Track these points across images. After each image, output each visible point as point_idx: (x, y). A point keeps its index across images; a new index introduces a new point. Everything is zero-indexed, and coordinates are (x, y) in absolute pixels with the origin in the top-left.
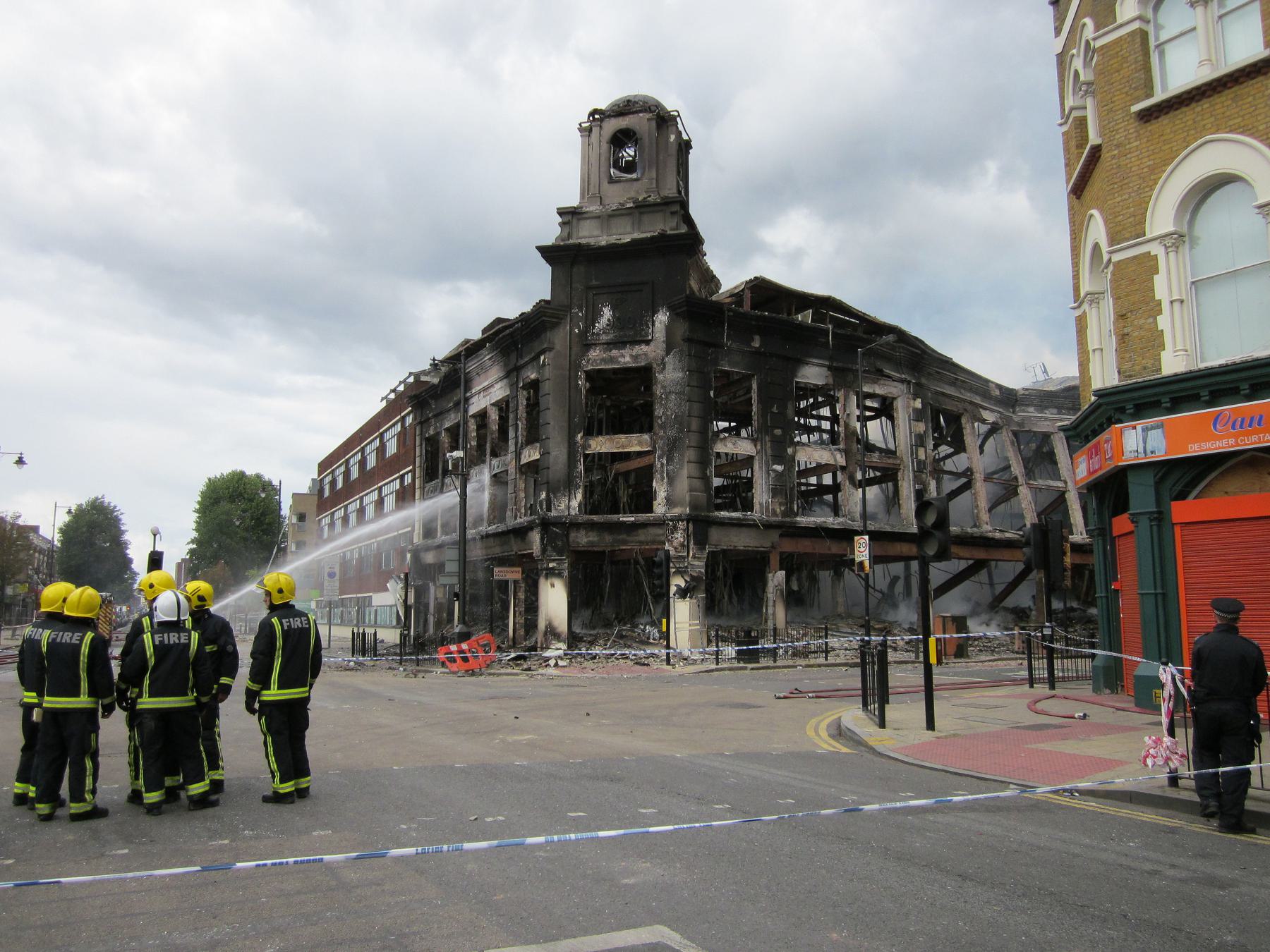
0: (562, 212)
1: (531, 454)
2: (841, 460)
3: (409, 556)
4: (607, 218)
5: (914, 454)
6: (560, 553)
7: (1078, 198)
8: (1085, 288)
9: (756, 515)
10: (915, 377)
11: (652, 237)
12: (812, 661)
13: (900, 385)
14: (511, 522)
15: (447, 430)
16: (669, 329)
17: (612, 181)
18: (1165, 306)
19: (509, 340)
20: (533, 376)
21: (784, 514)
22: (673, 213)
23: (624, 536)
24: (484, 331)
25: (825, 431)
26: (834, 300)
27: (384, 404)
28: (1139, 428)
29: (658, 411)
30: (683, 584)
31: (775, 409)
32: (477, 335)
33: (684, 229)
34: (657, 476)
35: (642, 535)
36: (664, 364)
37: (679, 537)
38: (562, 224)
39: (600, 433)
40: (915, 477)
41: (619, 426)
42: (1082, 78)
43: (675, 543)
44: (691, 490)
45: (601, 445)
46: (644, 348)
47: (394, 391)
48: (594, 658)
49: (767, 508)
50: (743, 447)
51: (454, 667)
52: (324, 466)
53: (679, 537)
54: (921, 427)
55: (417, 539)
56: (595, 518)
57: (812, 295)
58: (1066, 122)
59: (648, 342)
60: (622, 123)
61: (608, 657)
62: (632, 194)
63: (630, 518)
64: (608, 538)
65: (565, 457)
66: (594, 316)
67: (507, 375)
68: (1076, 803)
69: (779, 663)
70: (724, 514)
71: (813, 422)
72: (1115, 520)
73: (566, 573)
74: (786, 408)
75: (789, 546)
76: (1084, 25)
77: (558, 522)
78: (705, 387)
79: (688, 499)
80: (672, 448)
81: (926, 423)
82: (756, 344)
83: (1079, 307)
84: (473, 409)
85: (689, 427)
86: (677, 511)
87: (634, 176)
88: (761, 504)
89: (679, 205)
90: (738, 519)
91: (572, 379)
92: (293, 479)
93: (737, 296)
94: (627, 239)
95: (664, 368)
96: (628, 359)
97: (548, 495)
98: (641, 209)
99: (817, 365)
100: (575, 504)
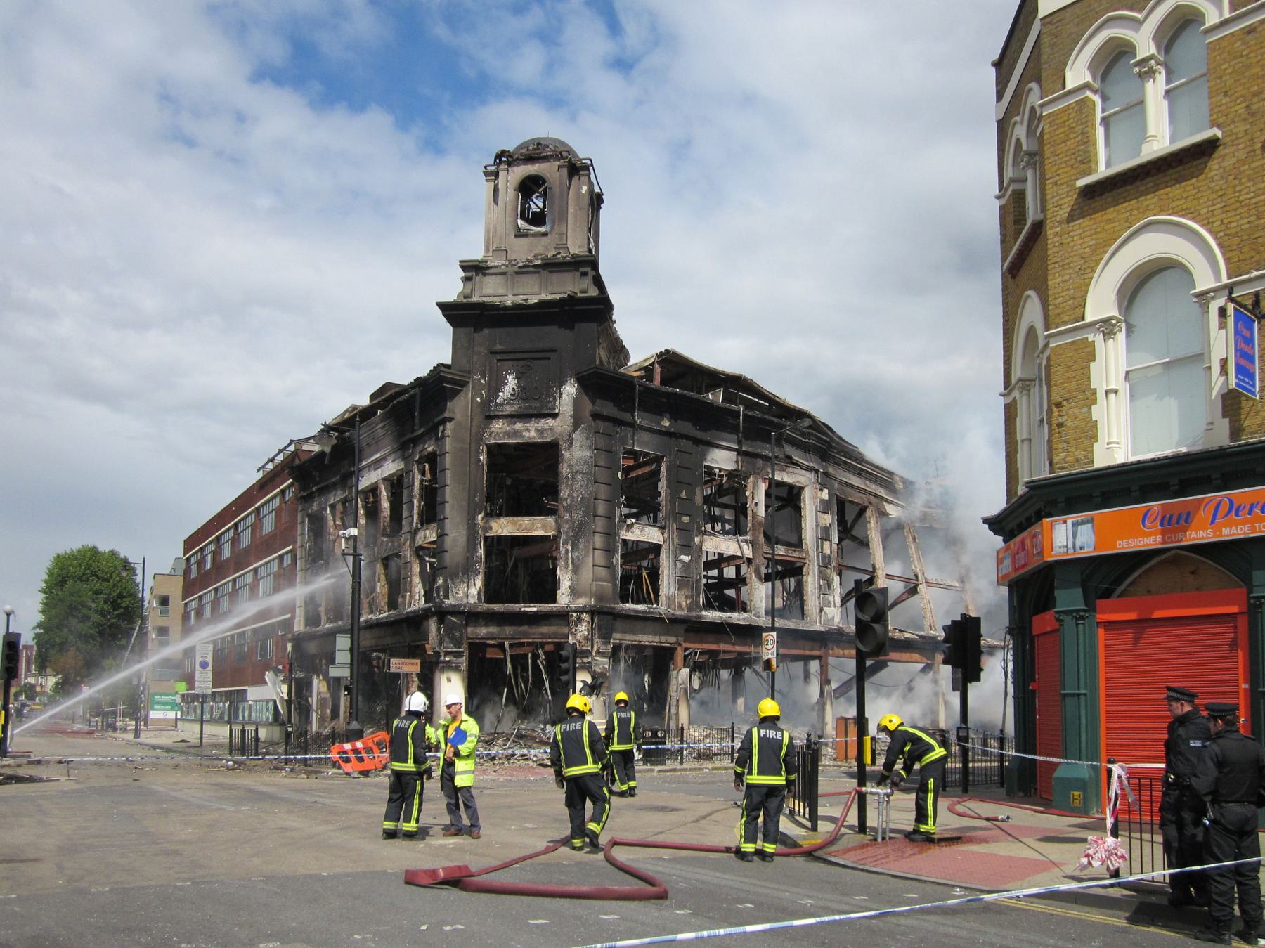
0: (465, 266)
2: (748, 552)
3: (289, 646)
5: (819, 549)
7: (1014, 277)
8: (1017, 373)
9: (662, 608)
10: (823, 467)
11: (562, 300)
12: (718, 764)
13: (808, 474)
16: (576, 402)
17: (520, 234)
18: (1100, 395)
19: (409, 411)
20: (430, 449)
21: (690, 608)
23: (525, 628)
24: (373, 397)
25: (728, 521)
26: (745, 379)
28: (1069, 522)
29: (564, 493)
30: (589, 681)
31: (683, 495)
32: (364, 402)
33: (594, 292)
34: (561, 563)
36: (571, 441)
37: (583, 629)
38: (466, 279)
39: (499, 515)
40: (820, 572)
41: (517, 509)
42: (1024, 147)
43: (579, 636)
45: (504, 527)
46: (550, 422)
47: (272, 460)
48: (493, 759)
50: (651, 535)
51: (348, 768)
52: (190, 543)
53: (583, 629)
54: (827, 519)
55: (299, 627)
56: (497, 607)
57: (723, 373)
58: (1003, 196)
59: (554, 416)
60: (532, 169)
61: (509, 757)
65: (465, 539)
66: (499, 384)
68: (1021, 904)
69: (685, 766)
70: (630, 606)
71: (717, 511)
72: (1036, 619)
73: (464, 667)
74: (695, 494)
76: (1030, 90)
77: (455, 611)
78: (612, 468)
81: (832, 515)
83: (1009, 394)
85: (595, 510)
86: (582, 602)
87: (543, 229)
89: (588, 264)
90: (644, 612)
92: (156, 558)
94: (534, 300)
96: (533, 433)
97: (445, 581)
98: (551, 266)
100: (474, 591)
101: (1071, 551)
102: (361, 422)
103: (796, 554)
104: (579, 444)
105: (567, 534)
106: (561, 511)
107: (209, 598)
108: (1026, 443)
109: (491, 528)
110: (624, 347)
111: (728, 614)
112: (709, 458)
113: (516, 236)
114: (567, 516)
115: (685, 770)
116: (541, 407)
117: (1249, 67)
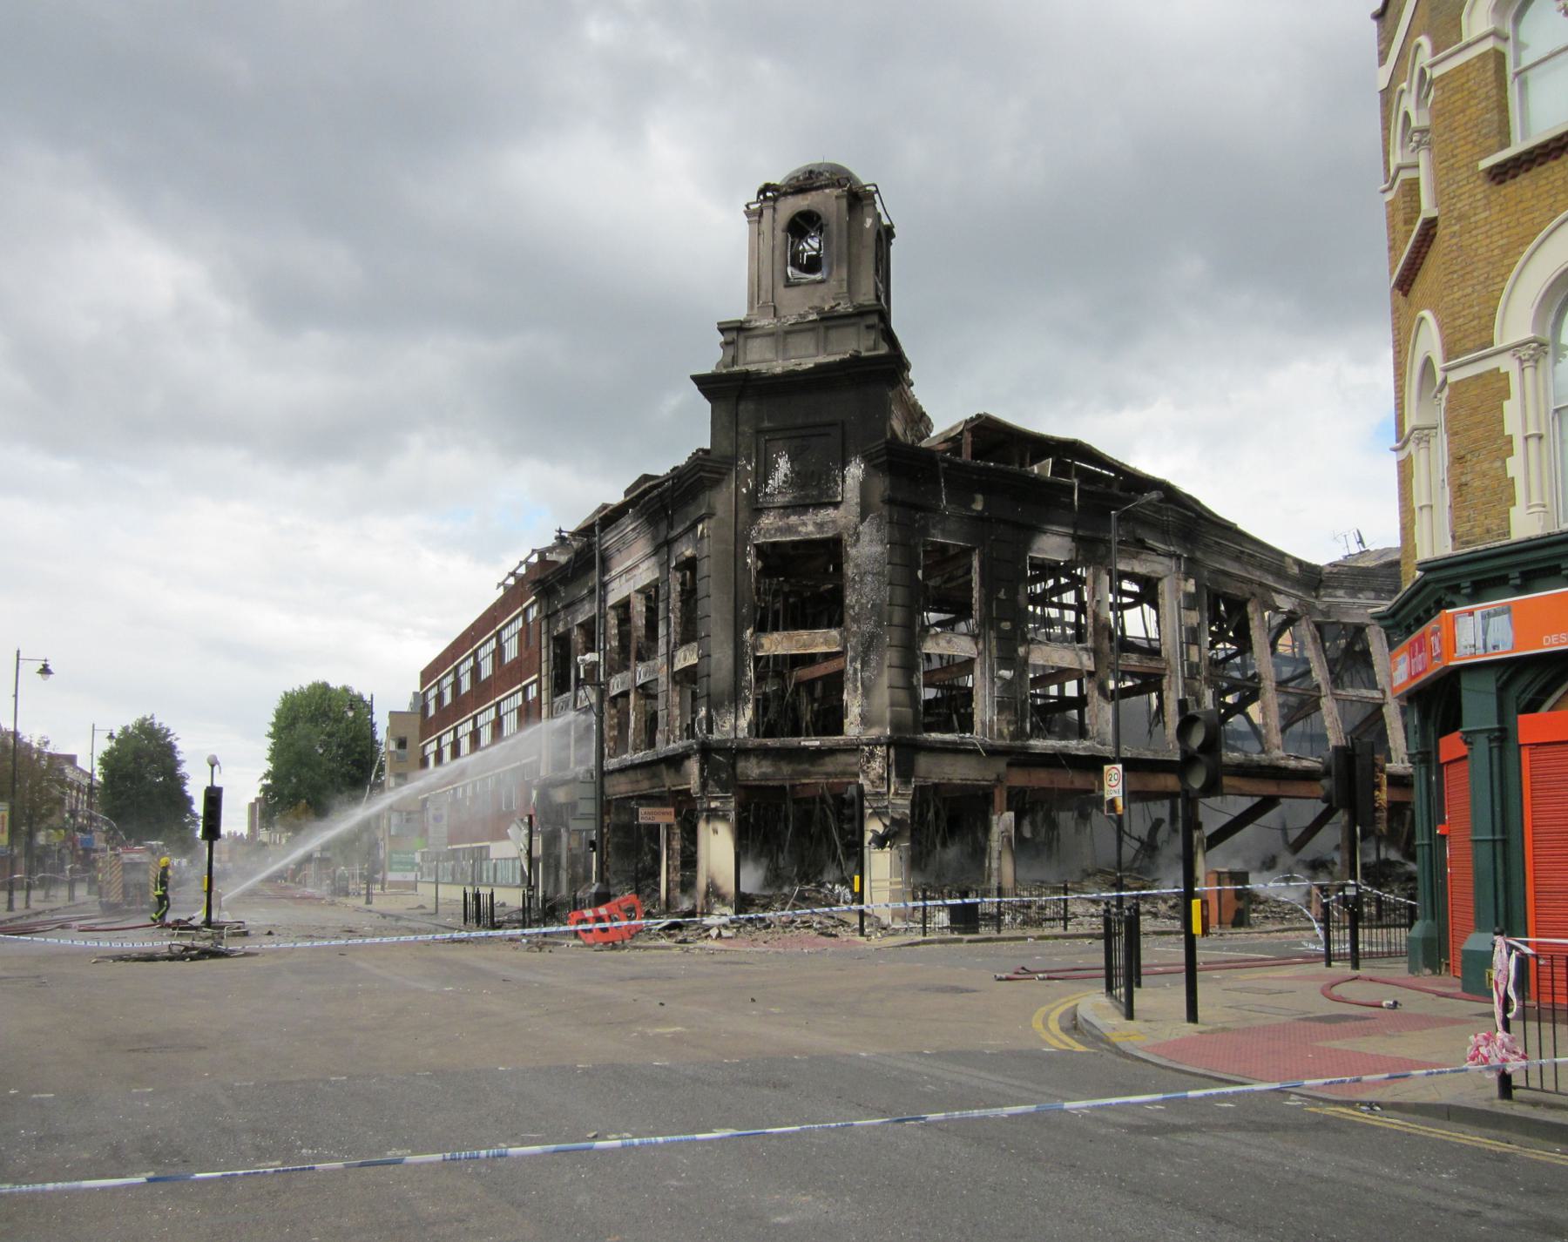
1: (686, 658)
2: (1088, 663)
4: (783, 337)
6: (724, 788)
7: (1405, 294)
9: (976, 737)
10: (1187, 551)
11: (842, 361)
12: (1047, 932)
13: (1166, 561)
15: (581, 625)
16: (864, 487)
17: (789, 284)
20: (688, 553)
21: (1014, 736)
22: (869, 327)
23: (806, 766)
24: (627, 493)
25: (1069, 624)
27: (501, 592)
28: (1478, 614)
29: (850, 598)
30: (881, 830)
31: (1002, 595)
32: (617, 498)
33: (883, 350)
34: (848, 686)
35: (830, 765)
36: (858, 535)
39: (776, 629)
42: (1414, 124)
43: (872, 775)
44: (892, 704)
45: (777, 644)
46: (831, 513)
47: (513, 574)
52: (428, 675)
53: (877, 766)
54: (1194, 618)
56: (770, 742)
57: (1052, 439)
59: (836, 505)
62: (816, 302)
63: (813, 742)
64: (786, 769)
67: (656, 552)
69: (1004, 934)
70: (935, 736)
72: (1443, 741)
73: (732, 816)
75: (1019, 778)
76: (1419, 46)
77: (721, 748)
79: (888, 715)
80: (869, 646)
81: (1201, 611)
82: (978, 506)
83: (1402, 448)
84: (612, 599)
86: (874, 732)
87: (818, 276)
88: (983, 723)
89: (878, 316)
90: (954, 743)
91: (738, 556)
93: (954, 441)
94: (809, 364)
95: (858, 540)
96: (810, 528)
97: (708, 712)
98: (829, 321)
100: (743, 723)
101: (1481, 651)
102: (602, 530)
103: (1153, 664)
104: (867, 538)
107: (448, 738)
108: (1425, 511)
109: (762, 646)
110: (924, 414)
114: (855, 628)
115: (1003, 939)
116: (820, 495)
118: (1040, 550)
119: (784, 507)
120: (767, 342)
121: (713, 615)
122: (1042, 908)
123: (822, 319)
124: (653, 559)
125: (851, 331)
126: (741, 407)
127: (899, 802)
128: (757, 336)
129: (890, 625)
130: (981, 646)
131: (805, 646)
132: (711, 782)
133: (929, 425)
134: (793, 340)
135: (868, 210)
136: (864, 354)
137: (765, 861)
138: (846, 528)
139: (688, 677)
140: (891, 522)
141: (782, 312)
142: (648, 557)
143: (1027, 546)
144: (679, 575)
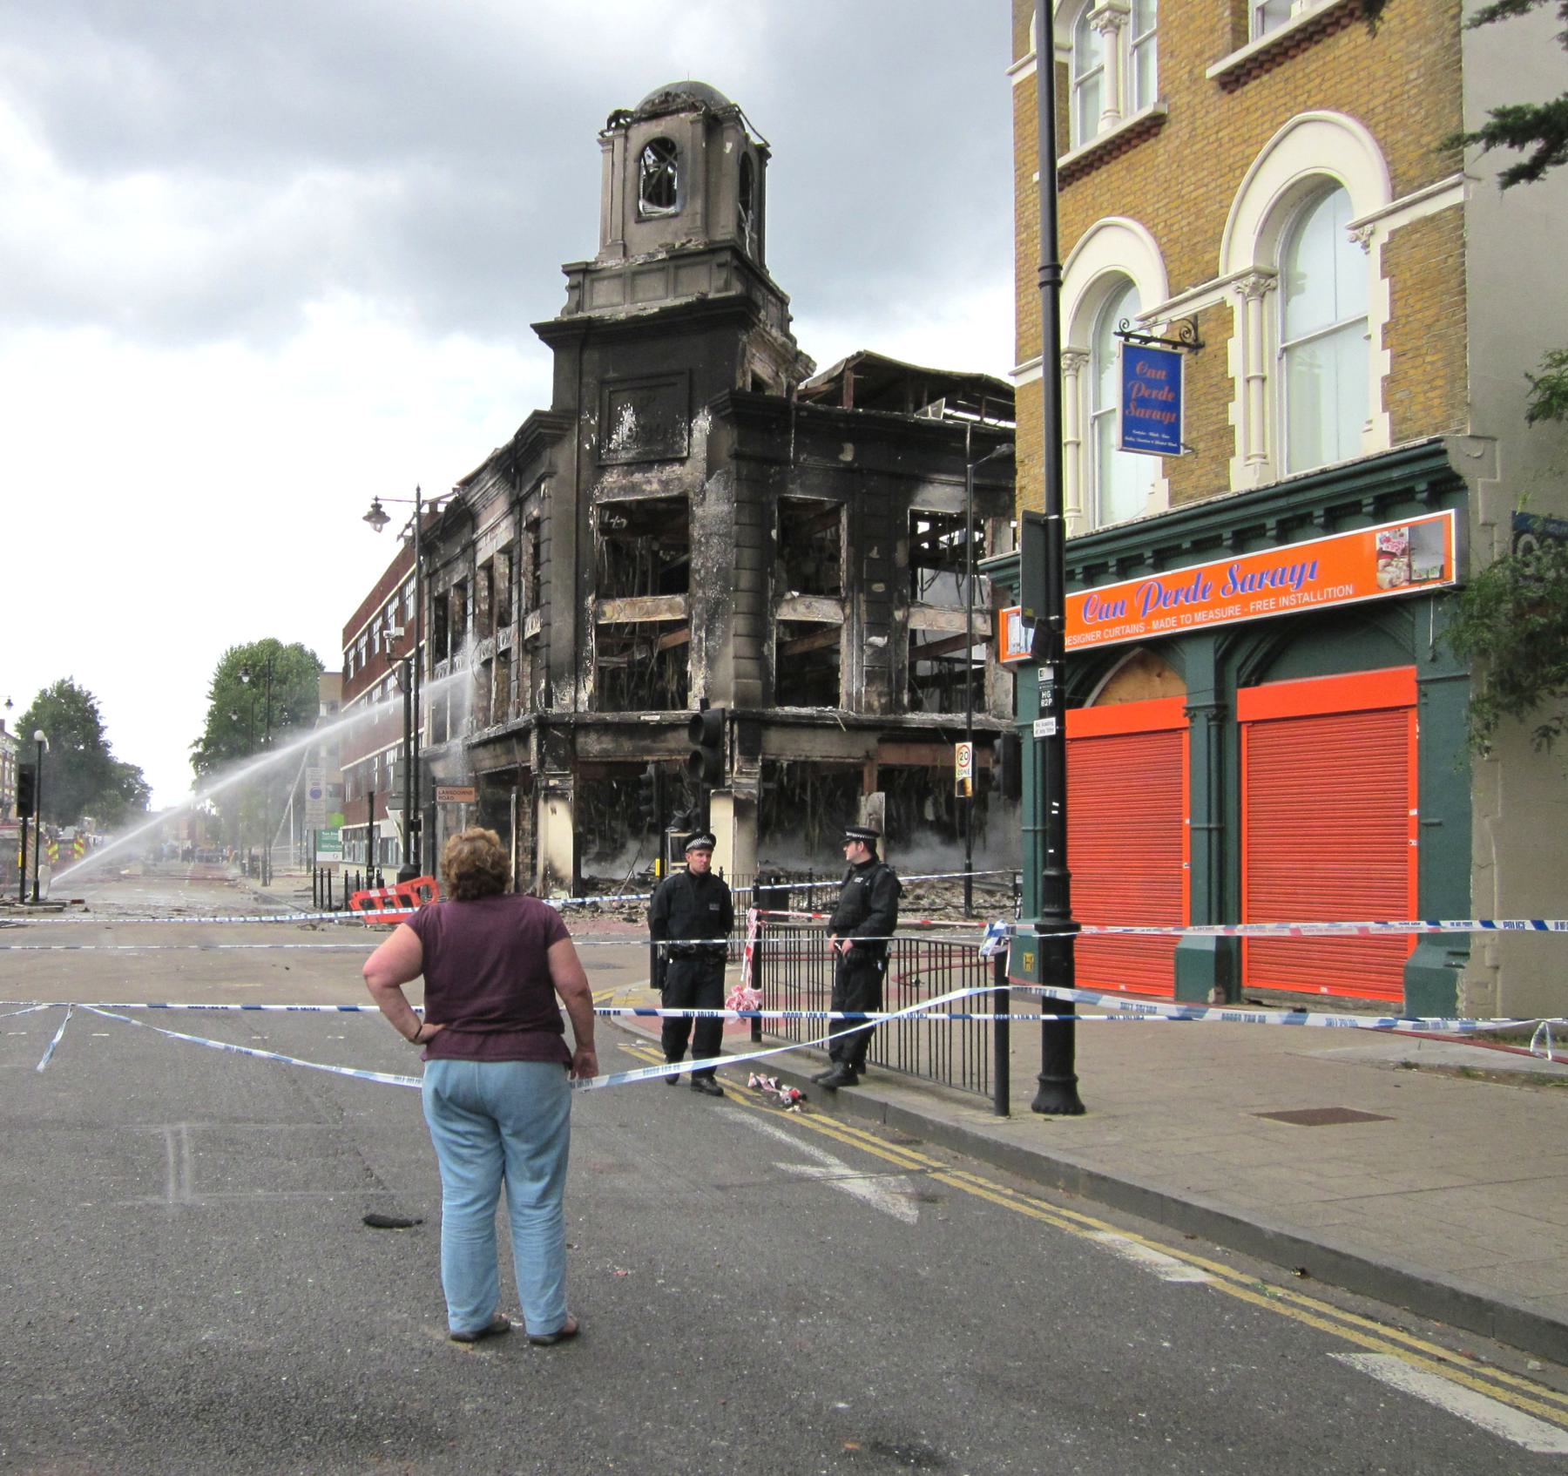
0: (569, 271)
1: (533, 627)
4: (630, 278)
6: (562, 766)
11: (688, 305)
14: (515, 722)
15: (455, 586)
16: (711, 440)
17: (640, 219)
20: (535, 513)
21: (886, 709)
22: (720, 266)
23: (647, 743)
27: (401, 544)
29: (696, 563)
31: (874, 554)
34: (693, 656)
36: (703, 492)
44: (737, 676)
45: (619, 612)
47: (408, 526)
49: (859, 702)
50: (824, 611)
52: (349, 631)
56: (609, 716)
59: (682, 461)
60: (656, 129)
62: (669, 240)
63: (653, 717)
64: (627, 745)
66: (609, 424)
67: (511, 511)
70: (790, 710)
73: (571, 794)
75: (894, 756)
77: (559, 723)
79: (732, 688)
80: (714, 612)
82: (847, 456)
84: (481, 559)
87: (672, 210)
88: (849, 695)
90: (811, 717)
91: (580, 515)
93: (835, 380)
94: (653, 309)
95: (704, 499)
96: (655, 486)
97: (548, 684)
98: (679, 259)
99: (948, 484)
100: (584, 696)
104: (714, 497)
105: (700, 616)
106: (693, 584)
109: (604, 614)
111: (949, 716)
112: (918, 499)
113: (637, 222)
114: (700, 594)
116: (665, 451)
117: (1192, 18)
118: (924, 503)
119: (628, 464)
120: (615, 285)
121: (553, 580)
122: (919, 898)
123: (671, 258)
124: (510, 518)
125: (702, 271)
126: (585, 356)
127: (744, 781)
128: (603, 279)
129: (736, 590)
130: (848, 611)
131: (648, 613)
132: (548, 759)
133: (809, 364)
134: (642, 281)
135: (730, 133)
136: (711, 296)
137: (917, 836)
138: (692, 486)
139: (531, 647)
140: (738, 479)
141: (633, 250)
142: (506, 515)
143: (908, 498)
144: (531, 536)
